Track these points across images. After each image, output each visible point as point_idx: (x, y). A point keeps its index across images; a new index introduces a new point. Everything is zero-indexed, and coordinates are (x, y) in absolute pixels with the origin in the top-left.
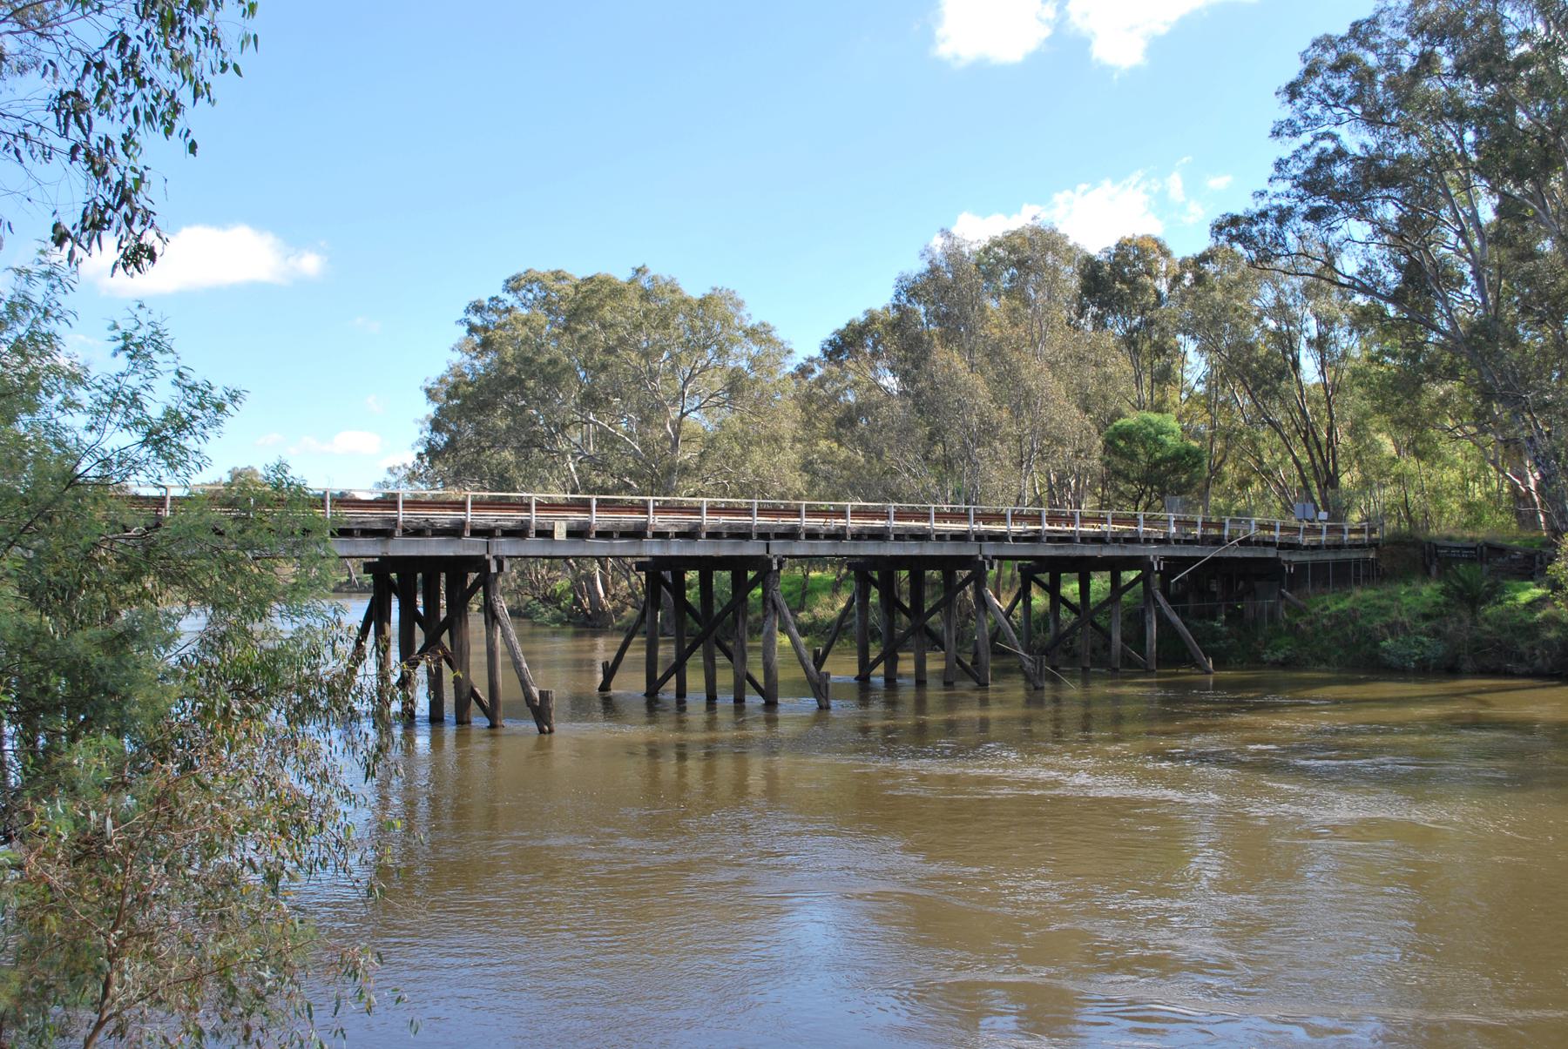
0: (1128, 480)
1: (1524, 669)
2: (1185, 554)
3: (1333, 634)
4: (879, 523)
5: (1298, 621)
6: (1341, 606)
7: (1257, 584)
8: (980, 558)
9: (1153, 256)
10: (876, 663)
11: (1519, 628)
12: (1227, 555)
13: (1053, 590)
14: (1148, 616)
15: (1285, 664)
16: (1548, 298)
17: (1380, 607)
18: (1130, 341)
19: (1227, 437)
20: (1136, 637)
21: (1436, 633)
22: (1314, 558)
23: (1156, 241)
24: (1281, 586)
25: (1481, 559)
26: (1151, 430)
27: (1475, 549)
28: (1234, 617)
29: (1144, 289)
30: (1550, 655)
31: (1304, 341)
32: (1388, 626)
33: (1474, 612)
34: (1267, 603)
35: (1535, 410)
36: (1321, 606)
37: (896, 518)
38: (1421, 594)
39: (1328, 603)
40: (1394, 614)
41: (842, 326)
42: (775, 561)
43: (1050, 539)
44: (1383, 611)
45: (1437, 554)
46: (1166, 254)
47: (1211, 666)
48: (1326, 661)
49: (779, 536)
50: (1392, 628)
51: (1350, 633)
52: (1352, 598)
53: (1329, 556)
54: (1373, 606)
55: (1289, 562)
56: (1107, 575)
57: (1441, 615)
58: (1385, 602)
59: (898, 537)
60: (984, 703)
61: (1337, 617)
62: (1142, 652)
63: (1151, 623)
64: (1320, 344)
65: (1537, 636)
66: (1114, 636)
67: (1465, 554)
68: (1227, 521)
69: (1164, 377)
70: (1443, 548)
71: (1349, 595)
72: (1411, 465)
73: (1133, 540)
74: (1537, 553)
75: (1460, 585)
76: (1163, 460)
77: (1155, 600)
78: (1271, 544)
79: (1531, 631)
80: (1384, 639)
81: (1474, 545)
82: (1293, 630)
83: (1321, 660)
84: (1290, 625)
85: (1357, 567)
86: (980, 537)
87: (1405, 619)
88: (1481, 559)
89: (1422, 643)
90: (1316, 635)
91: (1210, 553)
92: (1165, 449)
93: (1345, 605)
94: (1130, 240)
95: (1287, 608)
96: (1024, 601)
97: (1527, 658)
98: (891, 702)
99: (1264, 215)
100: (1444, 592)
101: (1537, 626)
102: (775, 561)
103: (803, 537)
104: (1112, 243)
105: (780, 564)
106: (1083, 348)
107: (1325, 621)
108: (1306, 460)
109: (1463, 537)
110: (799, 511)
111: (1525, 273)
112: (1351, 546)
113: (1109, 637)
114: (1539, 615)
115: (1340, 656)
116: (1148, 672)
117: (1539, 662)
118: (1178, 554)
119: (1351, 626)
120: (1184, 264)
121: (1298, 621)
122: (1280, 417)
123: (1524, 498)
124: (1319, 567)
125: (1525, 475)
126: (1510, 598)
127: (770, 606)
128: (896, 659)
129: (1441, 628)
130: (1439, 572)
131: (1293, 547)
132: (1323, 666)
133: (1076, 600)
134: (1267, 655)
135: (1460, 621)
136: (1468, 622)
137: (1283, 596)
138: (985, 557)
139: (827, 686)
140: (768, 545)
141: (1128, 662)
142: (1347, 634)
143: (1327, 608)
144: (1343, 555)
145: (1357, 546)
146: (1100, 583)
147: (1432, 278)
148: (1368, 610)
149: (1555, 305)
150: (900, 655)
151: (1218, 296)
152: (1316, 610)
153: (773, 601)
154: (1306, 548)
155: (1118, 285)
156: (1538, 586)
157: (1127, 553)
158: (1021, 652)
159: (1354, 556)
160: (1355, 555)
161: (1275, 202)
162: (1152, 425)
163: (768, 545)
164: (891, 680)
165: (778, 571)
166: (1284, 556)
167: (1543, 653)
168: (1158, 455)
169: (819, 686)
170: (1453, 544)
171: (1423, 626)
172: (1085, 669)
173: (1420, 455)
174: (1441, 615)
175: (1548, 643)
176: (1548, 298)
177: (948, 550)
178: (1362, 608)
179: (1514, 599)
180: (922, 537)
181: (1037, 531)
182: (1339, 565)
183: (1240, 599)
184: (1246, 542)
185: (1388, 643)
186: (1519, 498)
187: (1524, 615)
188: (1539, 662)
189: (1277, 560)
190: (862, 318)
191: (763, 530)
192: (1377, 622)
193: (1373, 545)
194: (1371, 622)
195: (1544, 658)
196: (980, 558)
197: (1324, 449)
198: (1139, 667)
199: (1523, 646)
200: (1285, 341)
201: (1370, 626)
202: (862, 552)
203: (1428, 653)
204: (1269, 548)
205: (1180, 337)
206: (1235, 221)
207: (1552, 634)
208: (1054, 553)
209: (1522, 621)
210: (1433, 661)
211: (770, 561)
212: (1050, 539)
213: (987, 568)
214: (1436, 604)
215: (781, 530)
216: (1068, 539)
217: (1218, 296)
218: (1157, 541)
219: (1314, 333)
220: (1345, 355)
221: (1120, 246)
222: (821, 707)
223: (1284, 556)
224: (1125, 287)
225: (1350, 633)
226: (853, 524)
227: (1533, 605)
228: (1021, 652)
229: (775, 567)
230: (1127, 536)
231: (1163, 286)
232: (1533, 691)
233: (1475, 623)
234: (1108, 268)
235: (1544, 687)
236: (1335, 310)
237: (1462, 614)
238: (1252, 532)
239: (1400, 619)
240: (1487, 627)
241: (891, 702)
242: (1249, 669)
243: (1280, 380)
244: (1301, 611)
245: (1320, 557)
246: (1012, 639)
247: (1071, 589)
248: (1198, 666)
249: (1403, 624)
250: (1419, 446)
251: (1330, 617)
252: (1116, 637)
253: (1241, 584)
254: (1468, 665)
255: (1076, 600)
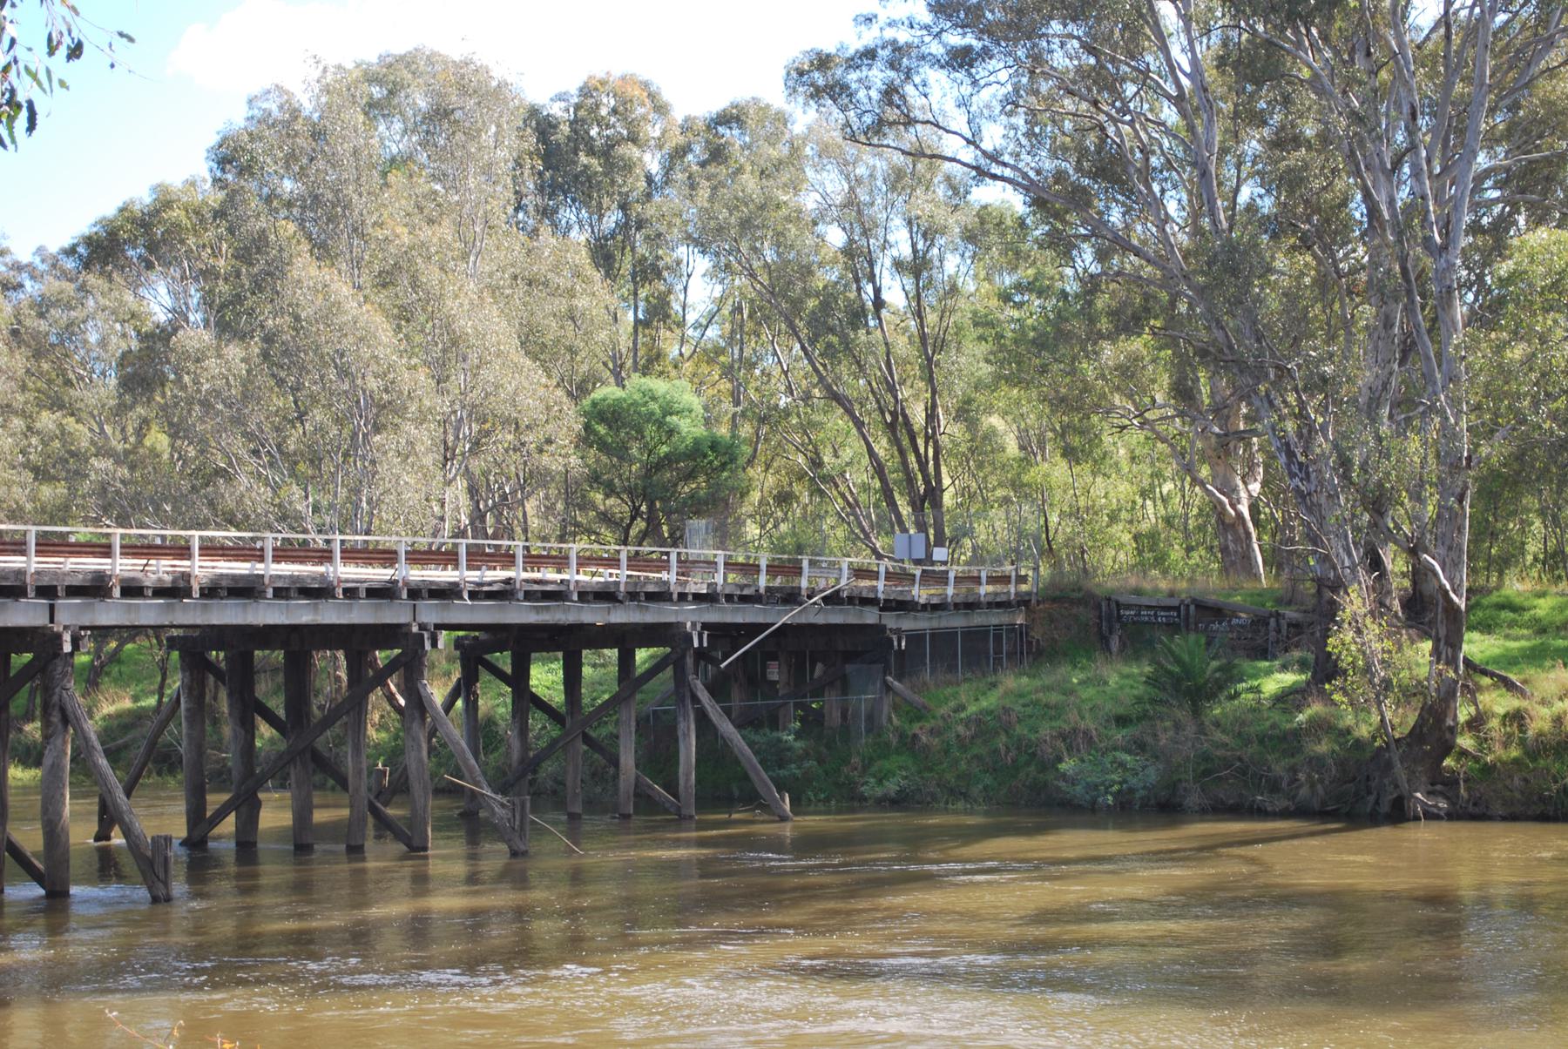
0: (610, 491)
1: (1281, 803)
2: (739, 619)
3: (975, 750)
4: (241, 568)
5: (916, 728)
6: (984, 704)
7: (849, 668)
8: (415, 629)
9: (640, 111)
10: (220, 815)
11: (1271, 738)
12: (803, 620)
13: (518, 680)
14: (682, 726)
15: (899, 802)
16: (1318, 210)
17: (1047, 706)
18: (603, 255)
19: (763, 420)
20: (659, 758)
21: (1139, 746)
22: (935, 624)
23: (645, 85)
24: (886, 671)
25: (1187, 627)
26: (654, 406)
27: (1177, 609)
28: (812, 723)
29: (628, 167)
30: (1321, 781)
31: (888, 262)
32: (1063, 736)
33: (1196, 712)
34: (864, 700)
35: (1305, 389)
36: (952, 704)
37: (277, 559)
38: (1106, 683)
39: (963, 699)
40: (1073, 716)
41: (110, 211)
42: (67, 637)
43: (529, 595)
44: (1054, 711)
45: (1119, 617)
46: (661, 109)
47: (787, 806)
48: (965, 796)
49: (73, 591)
50: (1071, 739)
51: (1003, 749)
52: (1001, 690)
53: (957, 622)
54: (1035, 703)
55: (898, 631)
56: (612, 654)
57: (1143, 716)
58: (1054, 698)
59: (280, 593)
60: (421, 883)
61: (979, 722)
62: (672, 787)
63: (686, 735)
64: (916, 267)
65: (1300, 750)
66: (622, 760)
67: (1162, 617)
68: (805, 564)
69: (659, 313)
70: (1129, 607)
71: (994, 685)
72: (1054, 470)
73: (661, 596)
74: (1271, 615)
75: (1177, 669)
76: (669, 460)
77: (695, 699)
78: (872, 602)
79: (1291, 741)
80: (1060, 760)
81: (1175, 602)
82: (909, 744)
83: (957, 793)
84: (902, 736)
85: (998, 638)
86: (415, 593)
87: (1089, 724)
88: (1187, 627)
89: (1122, 765)
90: (947, 752)
91: (788, 616)
92: (675, 439)
93: (990, 701)
94: (603, 83)
95: (895, 708)
96: (467, 702)
97: (1284, 785)
98: (248, 885)
99: (870, 54)
100: (1151, 681)
101: (1297, 734)
102: (67, 637)
103: (117, 592)
104: (573, 87)
105: (76, 642)
106: (540, 268)
107: (961, 729)
108: (891, 461)
109: (1156, 590)
110: (109, 546)
111: (1289, 170)
112: (990, 605)
113: (615, 762)
114: (1301, 717)
115: (986, 788)
116: (681, 820)
117: (1304, 792)
118: (729, 618)
119: (1003, 738)
120: (687, 127)
121: (916, 728)
122: (856, 386)
123: (1233, 525)
124: (943, 639)
125: (1235, 490)
126: (1251, 690)
127: (56, 718)
128: (256, 805)
129: (1149, 740)
130: (1123, 646)
131: (903, 606)
132: (960, 805)
133: (557, 697)
134: (870, 788)
135: (1178, 726)
136: (1190, 730)
137: (888, 688)
138: (422, 627)
139: (166, 860)
140: (52, 608)
141: (645, 802)
142: (996, 751)
143: (962, 708)
144: (977, 619)
145: (999, 605)
146: (599, 667)
147: (1138, 170)
148: (1029, 710)
149: (1328, 221)
150: (261, 796)
151: (749, 182)
152: (943, 710)
153: (63, 710)
154: (924, 607)
155: (583, 159)
156: (1284, 668)
157: (649, 618)
158: (487, 792)
159: (994, 621)
160: (995, 619)
161: (889, 34)
162: (654, 399)
163: (52, 608)
164: (247, 845)
165: (72, 654)
166: (890, 621)
167: (1309, 776)
168: (664, 449)
169: (151, 863)
170: (1145, 601)
171: (1119, 735)
172: (573, 817)
173: (1069, 453)
174: (1143, 716)
175: (1317, 762)
176: (1318, 210)
177: (361, 614)
178: (1018, 708)
179: (1257, 690)
180: (318, 592)
181: (508, 581)
182: (976, 636)
183: (817, 693)
184: (833, 599)
185: (1068, 765)
186: (1229, 527)
187: (1276, 716)
188: (1304, 792)
189: (879, 629)
190: (148, 200)
191: (45, 581)
192: (1045, 730)
193: (1023, 602)
194: (1035, 730)
195: (1313, 786)
196: (415, 629)
197: (920, 442)
198: (667, 812)
199: (1279, 768)
200: (858, 259)
201: (1033, 737)
202: (215, 621)
203: (1133, 781)
204: (867, 609)
205: (682, 251)
206: (823, 62)
207: (1323, 747)
208: (532, 618)
209: (1274, 726)
210: (1142, 793)
211: (58, 637)
212: (529, 595)
213: (428, 646)
214: (1139, 700)
215: (77, 581)
216: (557, 595)
217: (749, 182)
218: (698, 598)
219: (906, 251)
220: (953, 290)
221: (586, 91)
222: (155, 900)
223: (890, 621)
224: (594, 162)
225: (1003, 749)
226: (202, 569)
227: (1289, 699)
228: (487, 792)
229: (67, 648)
230: (651, 588)
231: (653, 163)
232: (1296, 842)
233: (1201, 730)
234: (566, 129)
235: (1312, 834)
236: (941, 216)
237: (1180, 714)
238: (843, 582)
239: (1082, 725)
240: (1219, 736)
241: (248, 885)
242: (839, 812)
243: (855, 328)
244: (918, 714)
245: (944, 624)
246: (471, 771)
247: (545, 677)
248: (765, 808)
249: (1086, 733)
250: (1076, 441)
251: (967, 722)
252: (628, 759)
253: (819, 669)
254: (1193, 799)
255: (557, 697)
